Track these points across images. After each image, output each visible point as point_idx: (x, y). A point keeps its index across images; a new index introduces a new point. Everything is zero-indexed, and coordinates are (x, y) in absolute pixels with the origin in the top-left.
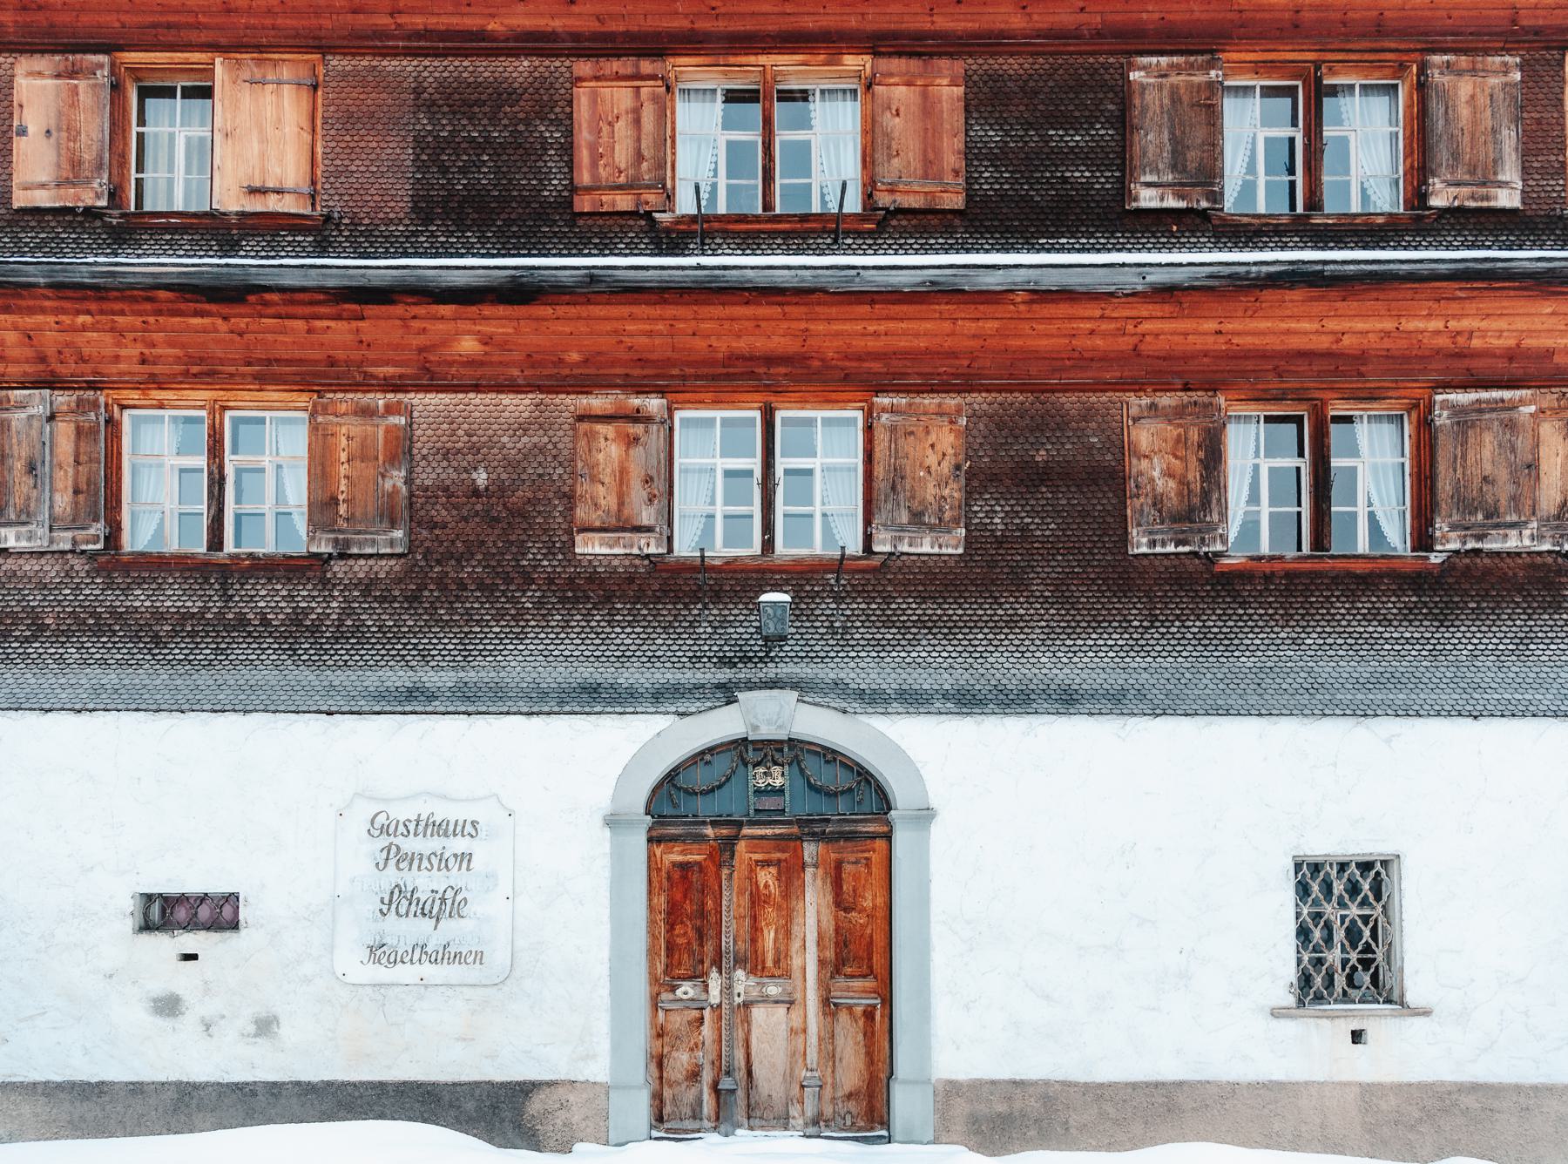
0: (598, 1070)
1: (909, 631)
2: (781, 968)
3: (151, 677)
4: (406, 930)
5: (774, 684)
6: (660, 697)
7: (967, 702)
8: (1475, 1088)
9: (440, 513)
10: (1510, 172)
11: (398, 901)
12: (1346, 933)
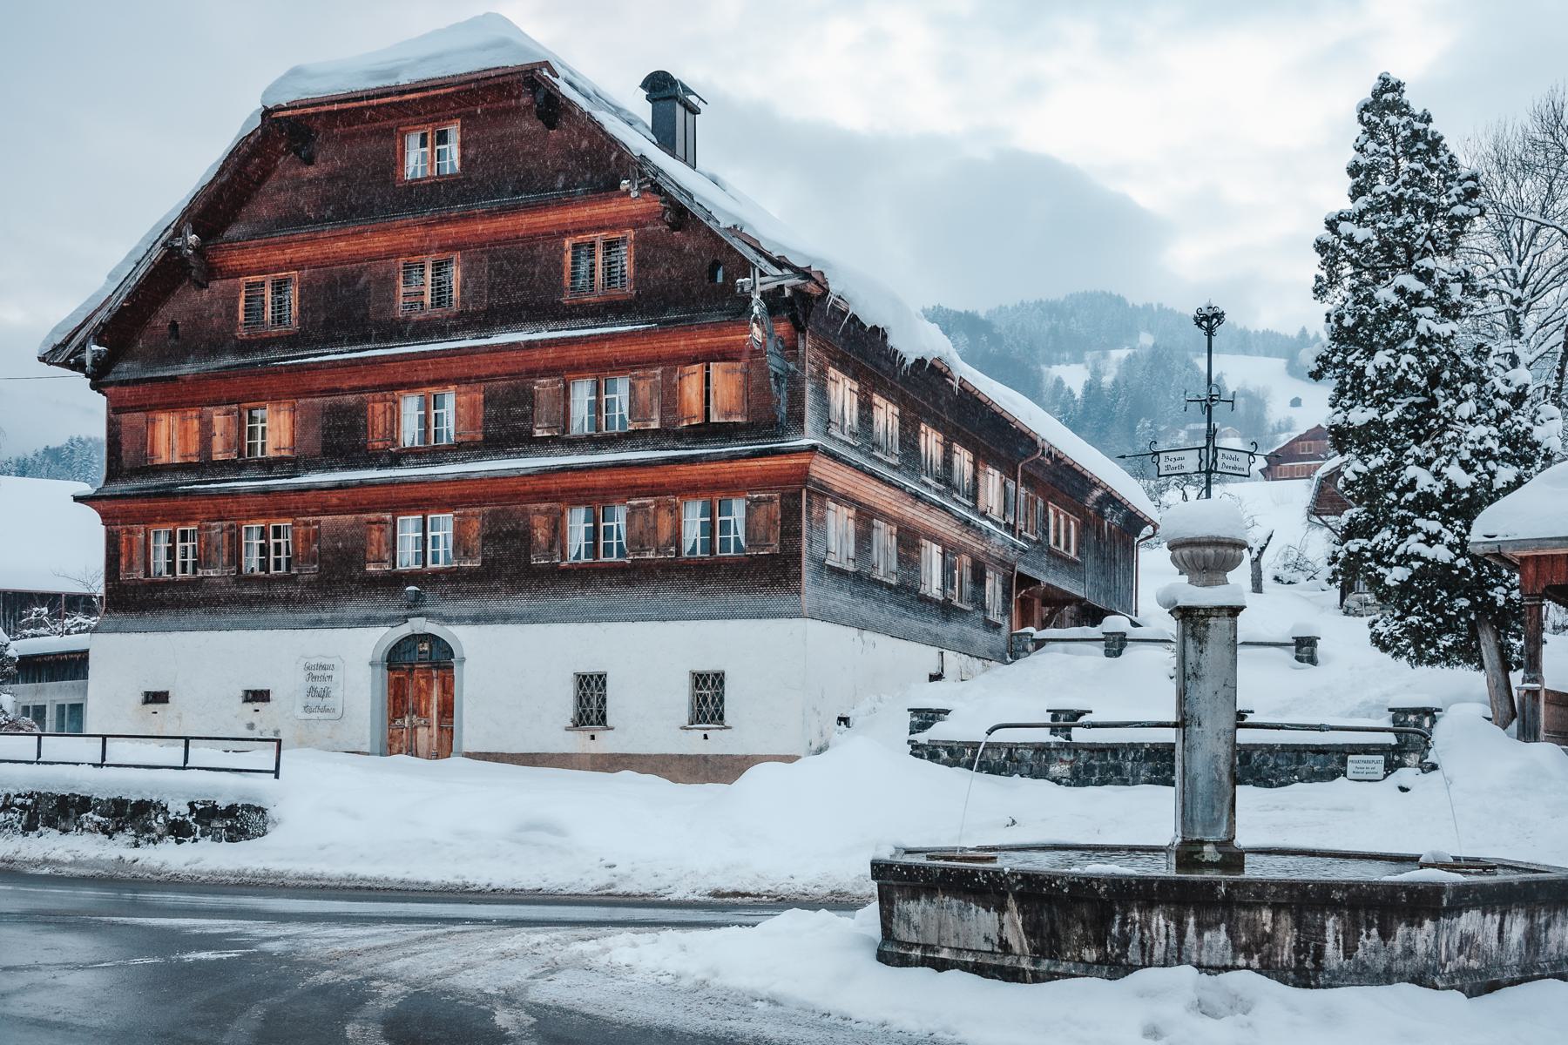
1: (470, 593)
2: (427, 714)
3: (246, 618)
4: (316, 701)
5: (420, 615)
6: (387, 621)
7: (476, 620)
9: (330, 557)
10: (656, 416)
11: (312, 692)
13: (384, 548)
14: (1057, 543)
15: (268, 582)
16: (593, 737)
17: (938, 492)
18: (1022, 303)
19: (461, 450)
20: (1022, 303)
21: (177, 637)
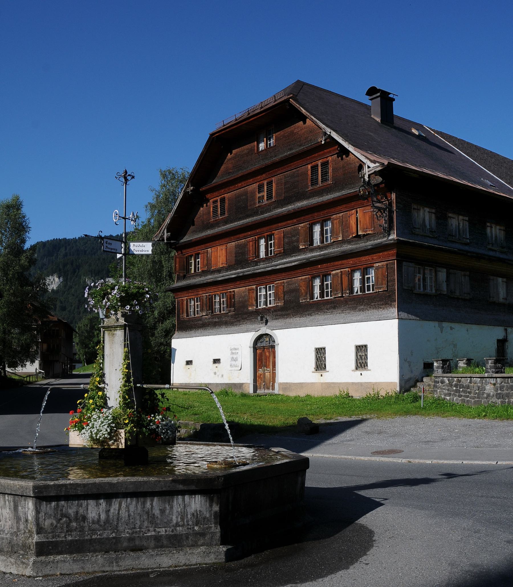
0: (249, 382)
10: (341, 235)
15: (220, 316)
16: (322, 375)
17: (501, 252)
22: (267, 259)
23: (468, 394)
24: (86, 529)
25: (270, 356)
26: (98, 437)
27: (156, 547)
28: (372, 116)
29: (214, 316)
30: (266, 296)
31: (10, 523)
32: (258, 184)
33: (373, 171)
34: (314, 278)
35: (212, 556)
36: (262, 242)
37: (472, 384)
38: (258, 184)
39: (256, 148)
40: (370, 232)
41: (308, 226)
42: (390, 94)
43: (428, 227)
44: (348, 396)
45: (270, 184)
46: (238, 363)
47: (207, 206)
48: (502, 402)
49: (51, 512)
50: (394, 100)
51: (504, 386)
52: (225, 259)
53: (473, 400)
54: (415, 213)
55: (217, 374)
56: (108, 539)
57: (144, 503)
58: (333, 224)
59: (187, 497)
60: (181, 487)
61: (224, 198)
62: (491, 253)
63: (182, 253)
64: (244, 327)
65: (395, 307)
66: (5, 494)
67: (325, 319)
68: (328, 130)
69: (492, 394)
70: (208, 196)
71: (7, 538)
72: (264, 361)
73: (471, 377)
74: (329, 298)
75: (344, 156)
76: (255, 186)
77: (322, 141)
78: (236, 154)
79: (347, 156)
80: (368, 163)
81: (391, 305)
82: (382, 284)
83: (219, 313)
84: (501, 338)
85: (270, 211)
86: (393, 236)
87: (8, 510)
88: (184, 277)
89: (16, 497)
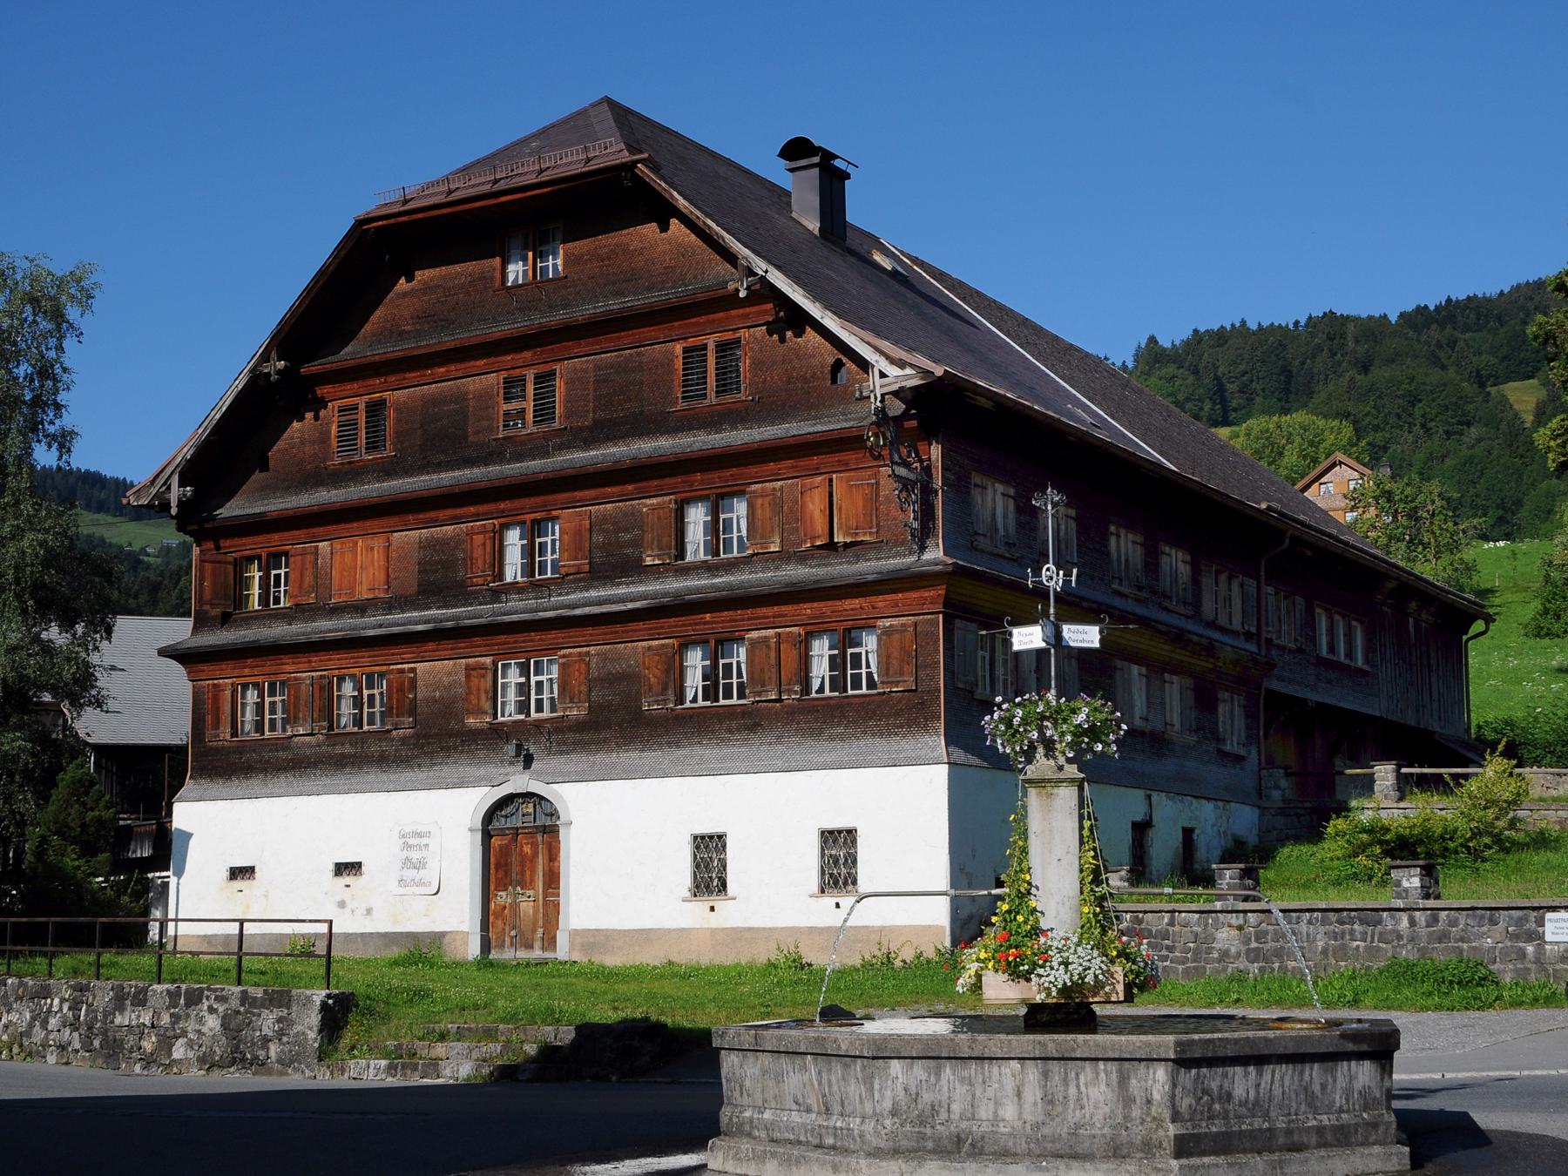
0: (465, 928)
4: (410, 874)
8: (750, 929)
11: (408, 863)
12: (709, 865)
13: (483, 697)
14: (1332, 649)
15: (359, 738)
16: (712, 909)
17: (1139, 601)
18: (1449, 300)
19: (564, 580)
20: (1449, 300)
21: (263, 804)
22: (533, 585)
23: (1164, 952)
24: (1231, 1115)
25: (535, 855)
26: (1076, 978)
27: (1320, 1146)
28: (794, 215)
29: (334, 736)
30: (523, 687)
31: (1107, 1109)
32: (504, 374)
33: (895, 387)
34: (685, 646)
35: (1395, 1160)
36: (514, 538)
37: (1177, 928)
38: (504, 374)
39: (498, 275)
40: (867, 538)
41: (673, 506)
42: (836, 157)
43: (1002, 532)
44: (800, 965)
45: (544, 379)
46: (430, 875)
47: (317, 418)
48: (1262, 970)
49: (1189, 1086)
50: (848, 176)
51: (1266, 933)
52: (382, 576)
53: (1181, 967)
54: (976, 494)
55: (350, 905)
56: (1260, 1130)
57: (1302, 1073)
58: (751, 507)
59: (1353, 1063)
60: (1350, 1047)
61: (382, 402)
62: (1118, 602)
63: (218, 548)
64: (448, 771)
65: (938, 735)
66: (1097, 1059)
67: (723, 759)
68: (760, 266)
69: (1233, 950)
70: (322, 391)
71: (1104, 1136)
72: (515, 869)
73: (1173, 912)
74: (734, 701)
75: (789, 334)
76: (493, 380)
77: (737, 291)
78: (427, 289)
79: (799, 334)
80: (881, 364)
81: (926, 729)
82: (902, 674)
83: (352, 729)
84: (1139, 818)
85: (545, 454)
86: (935, 554)
87: (1103, 1087)
88: (225, 620)
89: (1126, 1064)
